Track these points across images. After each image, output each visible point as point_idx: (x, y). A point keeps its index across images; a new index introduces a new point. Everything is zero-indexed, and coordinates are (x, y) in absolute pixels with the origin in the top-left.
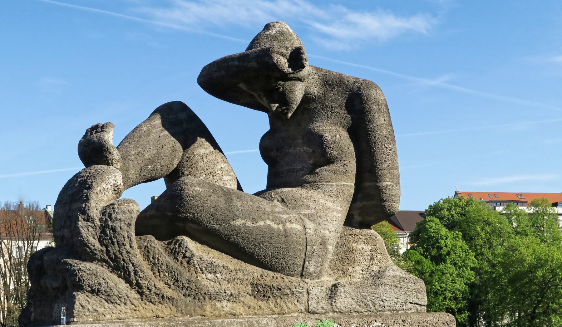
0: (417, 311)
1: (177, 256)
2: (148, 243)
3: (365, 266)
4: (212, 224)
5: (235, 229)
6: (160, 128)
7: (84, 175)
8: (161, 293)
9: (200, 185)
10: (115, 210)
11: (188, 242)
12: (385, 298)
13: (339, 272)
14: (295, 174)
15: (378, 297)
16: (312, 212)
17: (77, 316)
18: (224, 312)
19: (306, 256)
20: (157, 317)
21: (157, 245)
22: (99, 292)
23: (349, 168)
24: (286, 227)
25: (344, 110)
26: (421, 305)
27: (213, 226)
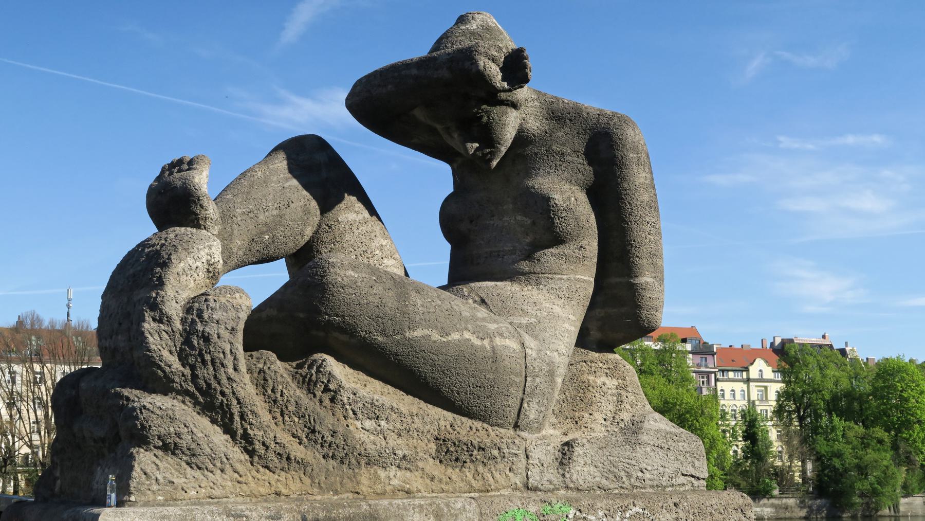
0: (692, 488)
1: (314, 389)
2: (265, 363)
3: (609, 412)
4: (374, 336)
5: (411, 344)
6: (284, 174)
7: (157, 243)
8: (286, 452)
9: (355, 267)
10: (209, 305)
11: (332, 365)
12: (646, 466)
13: (568, 421)
14: (500, 259)
15: (635, 464)
16: (531, 322)
17: (135, 492)
18: (391, 487)
19: (524, 394)
20: (278, 495)
21: (280, 368)
22: (177, 449)
23: (587, 254)
24: (494, 344)
25: (583, 159)
26: (698, 479)
27: (375, 339)
